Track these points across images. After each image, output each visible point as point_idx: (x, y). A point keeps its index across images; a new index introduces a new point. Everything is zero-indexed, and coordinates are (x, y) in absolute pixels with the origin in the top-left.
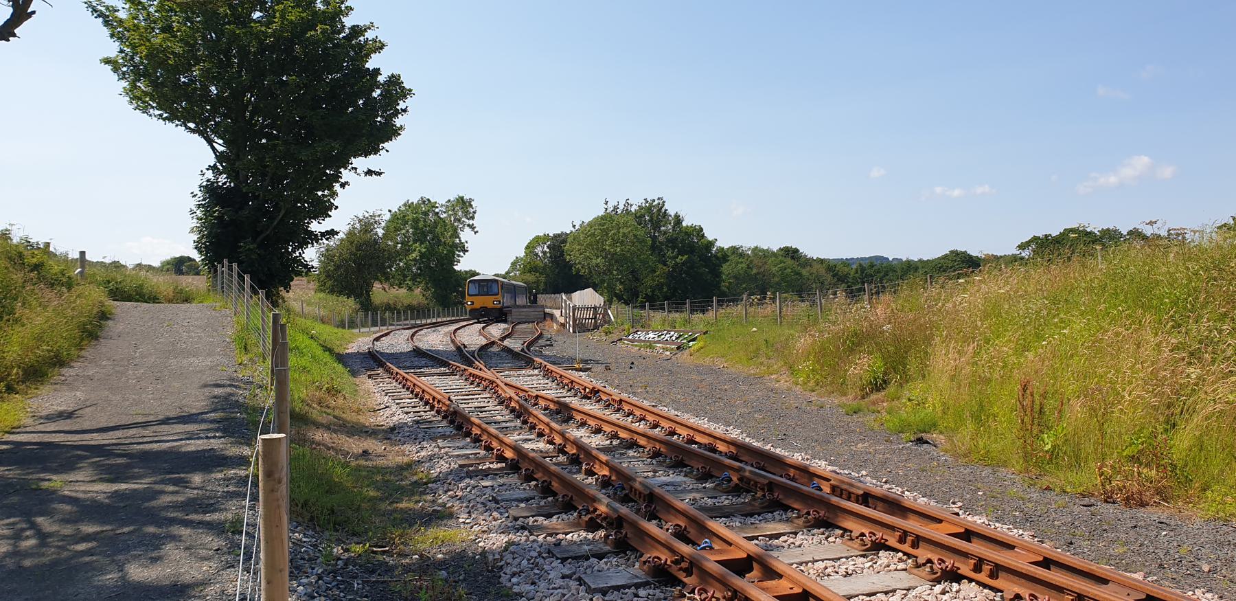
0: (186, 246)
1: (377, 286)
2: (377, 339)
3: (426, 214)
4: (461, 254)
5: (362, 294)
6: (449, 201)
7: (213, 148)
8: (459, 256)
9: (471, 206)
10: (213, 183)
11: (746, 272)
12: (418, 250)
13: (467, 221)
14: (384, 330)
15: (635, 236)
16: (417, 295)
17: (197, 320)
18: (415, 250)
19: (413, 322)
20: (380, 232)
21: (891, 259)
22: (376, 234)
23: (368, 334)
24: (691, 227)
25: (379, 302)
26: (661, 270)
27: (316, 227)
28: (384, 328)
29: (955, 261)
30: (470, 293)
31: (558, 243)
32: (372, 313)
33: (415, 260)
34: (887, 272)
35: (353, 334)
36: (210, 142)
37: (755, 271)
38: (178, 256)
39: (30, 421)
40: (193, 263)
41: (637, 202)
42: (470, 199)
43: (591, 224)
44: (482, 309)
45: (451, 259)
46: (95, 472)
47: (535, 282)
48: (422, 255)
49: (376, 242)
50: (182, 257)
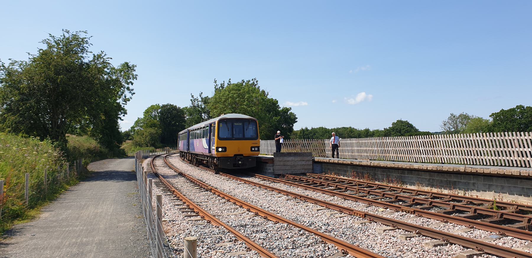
30: (221, 136)
44: (238, 158)
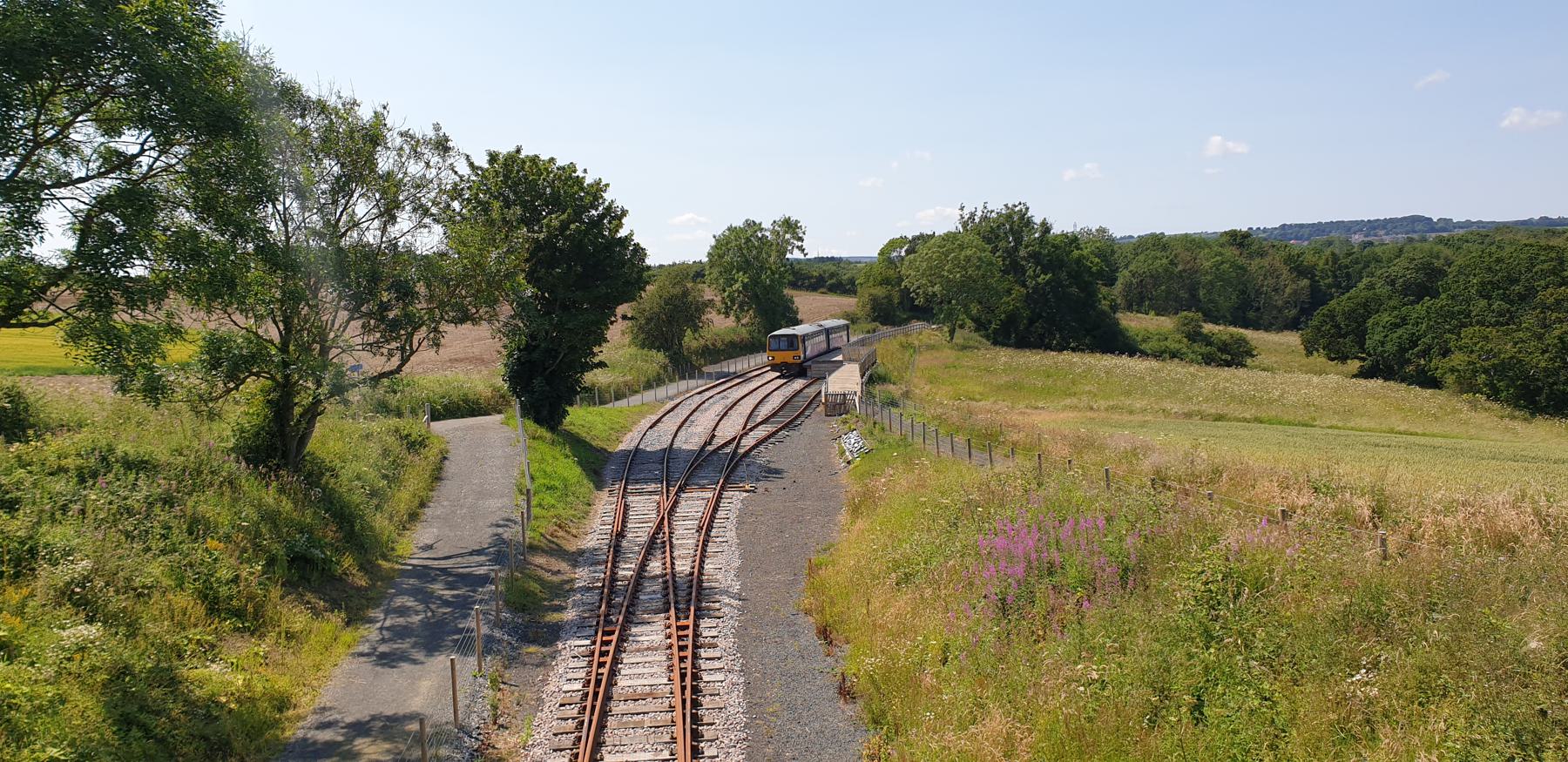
11: (1166, 270)
15: (980, 259)
18: (737, 281)
21: (1435, 220)
26: (1018, 291)
29: (1408, 269)
33: (737, 290)
34: (1369, 262)
37: (1180, 267)
39: (416, 550)
41: (997, 205)
47: (886, 297)
48: (745, 286)
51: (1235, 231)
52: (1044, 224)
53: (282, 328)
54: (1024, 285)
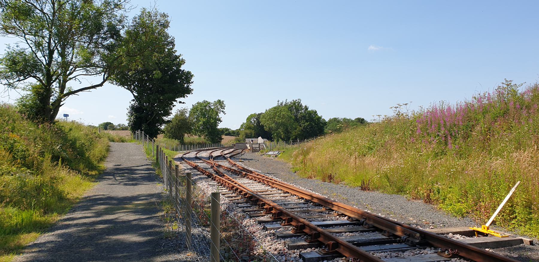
0: (126, 123)
1: (186, 135)
2: (185, 154)
3: (205, 106)
4: (219, 122)
5: (180, 139)
6: (215, 101)
7: (133, 94)
8: (218, 123)
9: (223, 103)
10: (133, 105)
12: (202, 120)
13: (221, 110)
14: (188, 151)
16: (202, 139)
17: (133, 147)
19: (199, 149)
20: (187, 115)
22: (186, 116)
23: (182, 153)
24: (311, 111)
25: (187, 141)
27: (165, 118)
28: (188, 151)
31: (258, 116)
32: (184, 145)
35: (177, 153)
36: (132, 92)
38: (106, 122)
40: (112, 125)
41: (290, 100)
42: (223, 101)
43: (270, 110)
45: (216, 125)
46: (39, 233)
48: (204, 123)
49: (186, 119)
50: (107, 122)
51: (359, 118)
52: (306, 106)
53: (47, 59)
54: (300, 126)
